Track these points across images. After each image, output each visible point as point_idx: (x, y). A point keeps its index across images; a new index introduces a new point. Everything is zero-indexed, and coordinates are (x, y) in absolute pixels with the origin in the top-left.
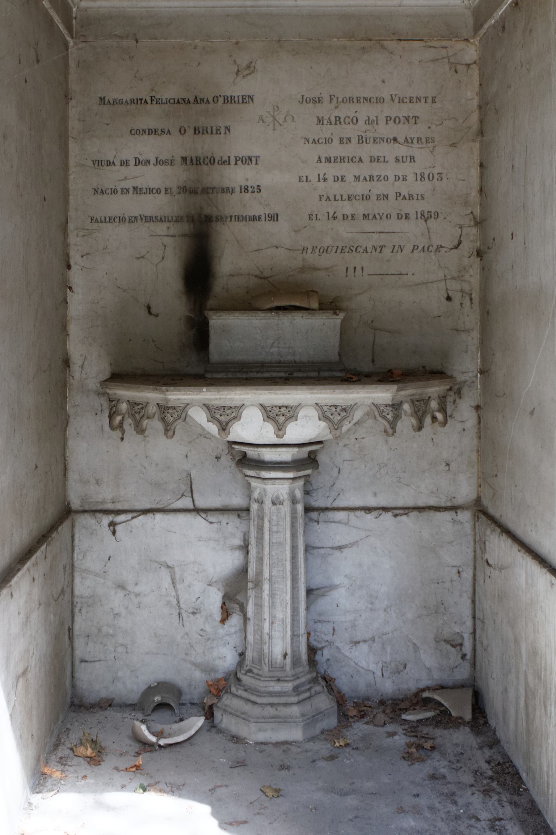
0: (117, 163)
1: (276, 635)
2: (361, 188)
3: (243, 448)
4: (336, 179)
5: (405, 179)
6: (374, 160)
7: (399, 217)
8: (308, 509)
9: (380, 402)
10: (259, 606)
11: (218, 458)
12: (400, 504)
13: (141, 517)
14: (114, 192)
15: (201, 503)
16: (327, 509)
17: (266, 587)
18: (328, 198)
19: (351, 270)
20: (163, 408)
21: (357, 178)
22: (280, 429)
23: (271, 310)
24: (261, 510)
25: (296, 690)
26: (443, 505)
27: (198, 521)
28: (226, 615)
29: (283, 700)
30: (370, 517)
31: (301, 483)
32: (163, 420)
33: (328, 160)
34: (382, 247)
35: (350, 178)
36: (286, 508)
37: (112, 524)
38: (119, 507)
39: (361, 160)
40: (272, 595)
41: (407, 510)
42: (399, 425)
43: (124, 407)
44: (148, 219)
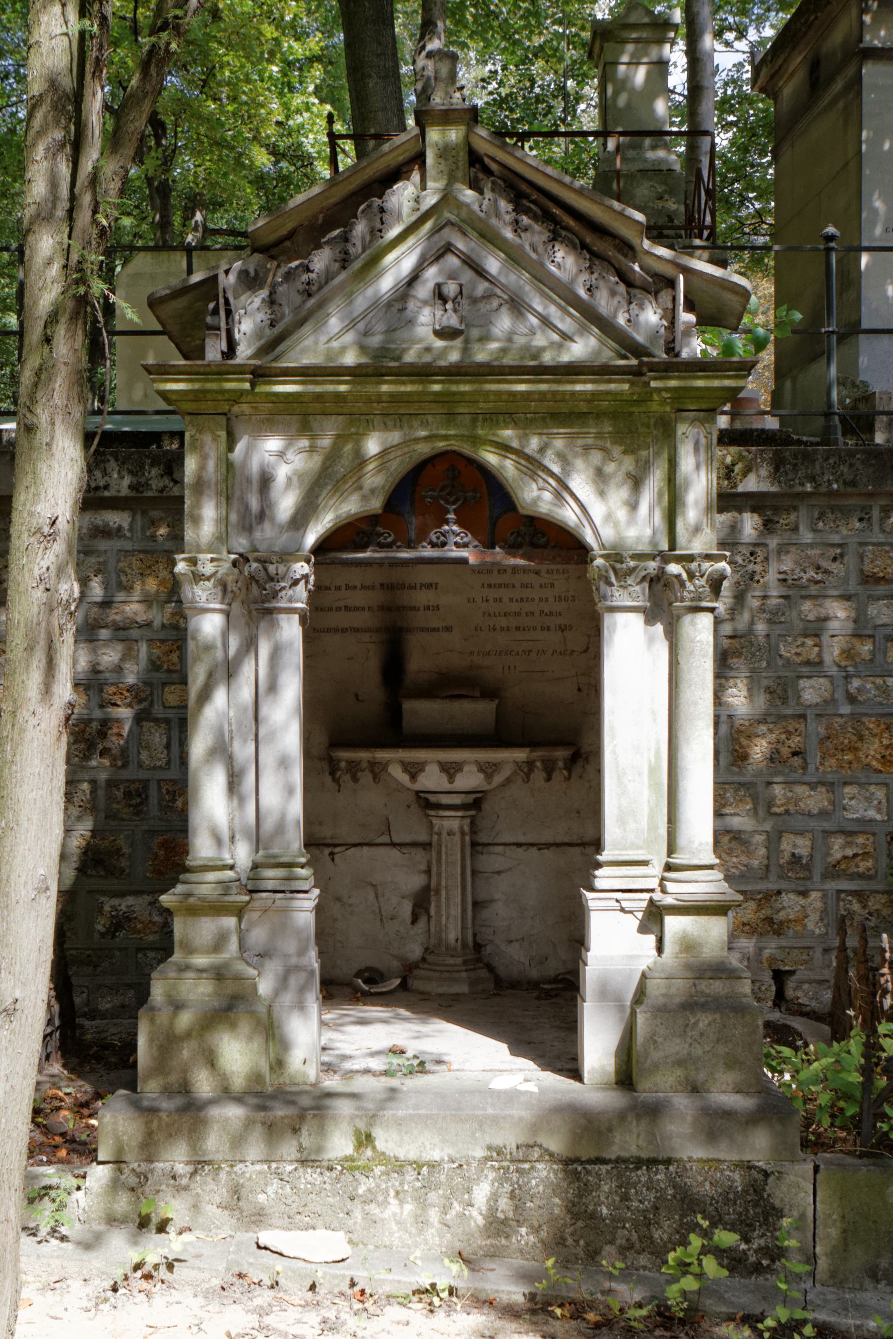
0: (333, 588)
1: (451, 926)
2: (514, 607)
3: (427, 796)
4: (495, 600)
5: (547, 600)
6: (524, 586)
7: (542, 629)
8: (474, 844)
9: (519, 760)
10: (438, 907)
11: (409, 806)
12: (543, 841)
13: (353, 849)
14: (330, 609)
15: (396, 839)
16: (489, 844)
17: (443, 892)
18: (490, 615)
19: (506, 668)
20: (372, 764)
21: (511, 600)
22: (451, 779)
23: (446, 697)
24: (440, 840)
25: (465, 962)
26: (575, 842)
27: (395, 853)
28: (414, 921)
29: (456, 968)
30: (520, 850)
31: (468, 821)
32: (372, 771)
33: (490, 586)
34: (530, 651)
35: (506, 599)
36: (457, 838)
37: (332, 854)
38: (337, 842)
39: (514, 586)
40: (448, 899)
41: (548, 846)
42: (532, 776)
43: (343, 764)
44: (356, 630)
